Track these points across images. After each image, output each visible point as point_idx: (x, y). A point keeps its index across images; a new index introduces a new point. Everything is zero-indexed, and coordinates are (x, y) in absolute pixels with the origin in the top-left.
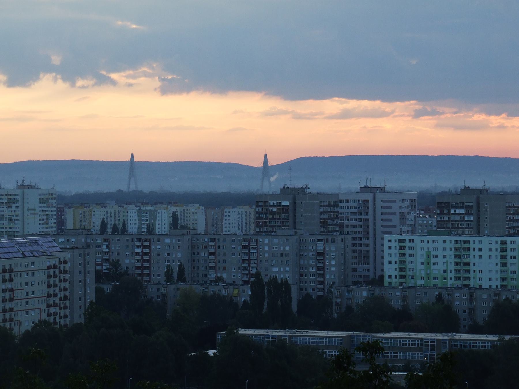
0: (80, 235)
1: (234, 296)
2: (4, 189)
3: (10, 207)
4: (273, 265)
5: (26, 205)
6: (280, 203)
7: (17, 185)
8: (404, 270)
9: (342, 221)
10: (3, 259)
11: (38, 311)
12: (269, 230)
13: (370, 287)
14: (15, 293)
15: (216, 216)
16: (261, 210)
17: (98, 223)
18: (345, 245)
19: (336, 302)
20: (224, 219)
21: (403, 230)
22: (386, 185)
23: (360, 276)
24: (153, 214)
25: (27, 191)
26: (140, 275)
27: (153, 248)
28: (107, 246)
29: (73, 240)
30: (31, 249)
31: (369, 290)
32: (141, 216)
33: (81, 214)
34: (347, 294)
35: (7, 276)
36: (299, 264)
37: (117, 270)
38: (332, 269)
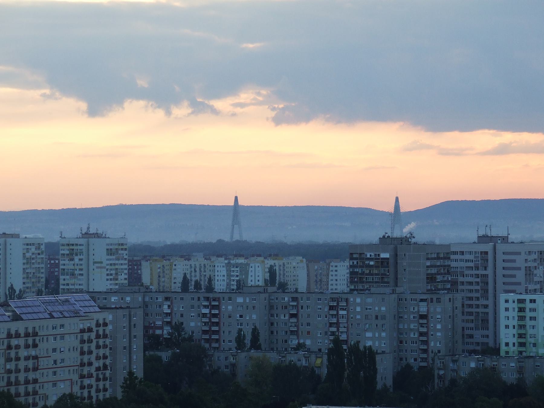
0: (136, 293)
1: (317, 367)
2: (65, 238)
3: (72, 260)
4: (366, 329)
5: (91, 257)
6: (379, 255)
7: (81, 233)
8: (523, 336)
9: (455, 277)
10: (26, 320)
11: (68, 383)
12: (365, 288)
13: (480, 356)
14: (40, 361)
15: (320, 271)
16: (355, 263)
17: (180, 279)
18: (453, 305)
19: (439, 374)
20: (330, 275)
21: (529, 288)
22: (509, 233)
23: (478, 344)
24: (244, 269)
25: (92, 240)
26: (207, 341)
27: (223, 309)
28: (168, 306)
29: (128, 299)
30: (61, 308)
31: (478, 360)
32: (230, 271)
33: (159, 268)
34: (451, 365)
35: (30, 341)
36: (398, 328)
37: (180, 335)
38: (437, 335)
